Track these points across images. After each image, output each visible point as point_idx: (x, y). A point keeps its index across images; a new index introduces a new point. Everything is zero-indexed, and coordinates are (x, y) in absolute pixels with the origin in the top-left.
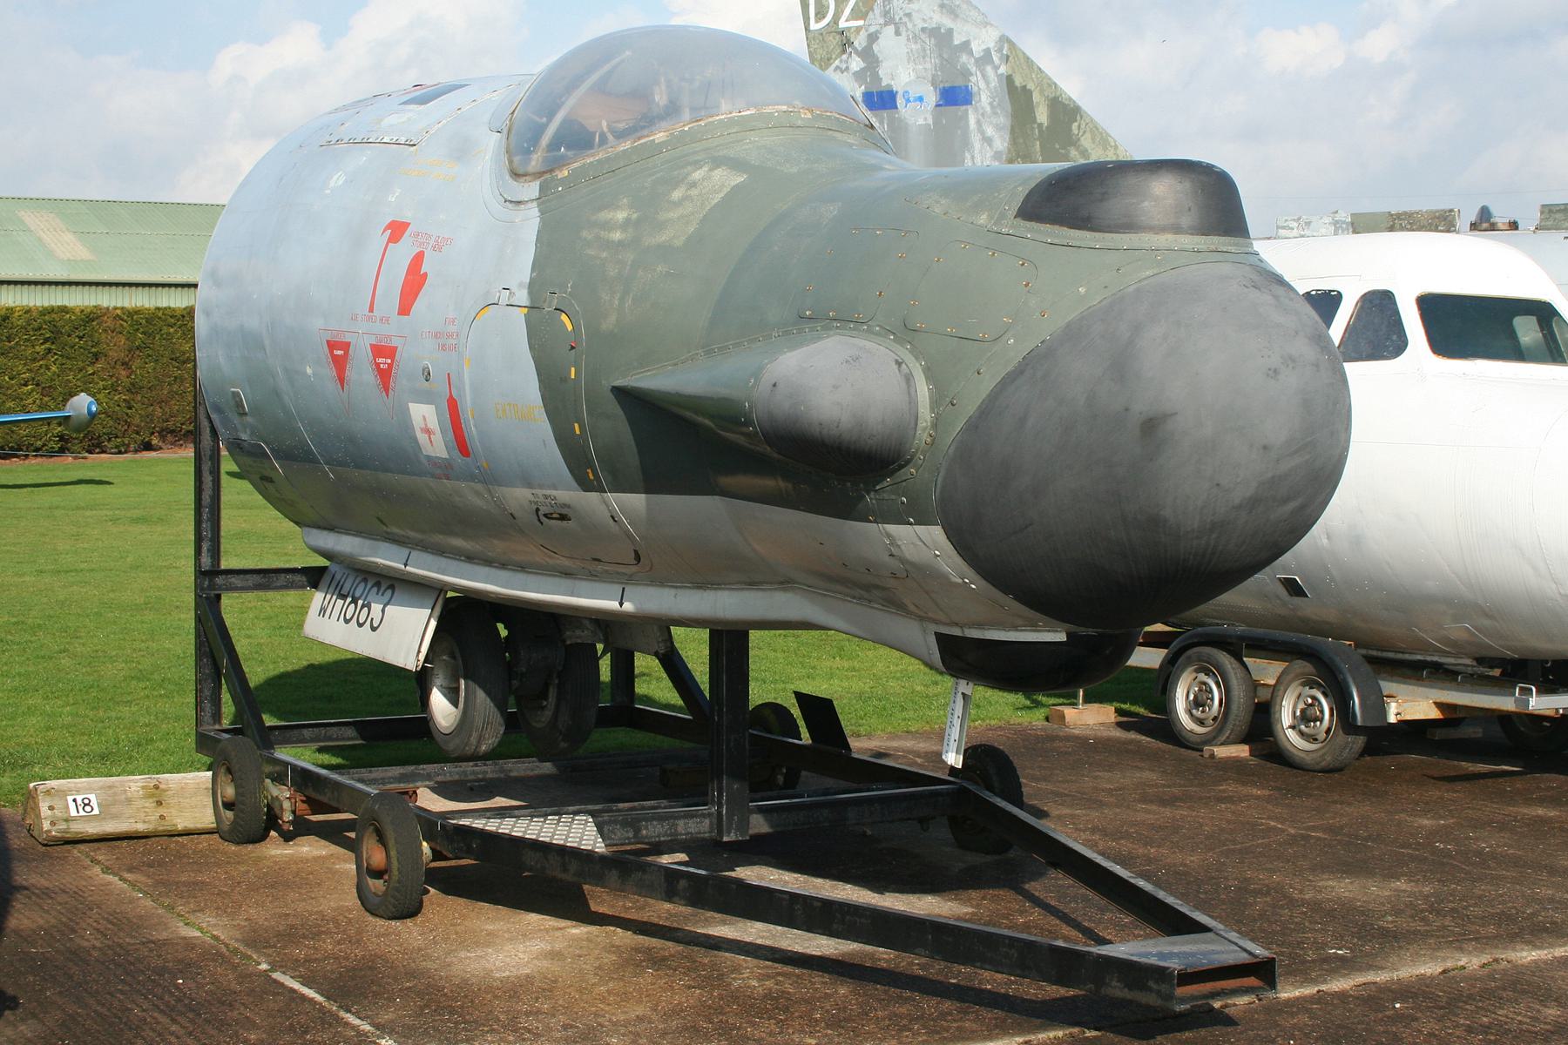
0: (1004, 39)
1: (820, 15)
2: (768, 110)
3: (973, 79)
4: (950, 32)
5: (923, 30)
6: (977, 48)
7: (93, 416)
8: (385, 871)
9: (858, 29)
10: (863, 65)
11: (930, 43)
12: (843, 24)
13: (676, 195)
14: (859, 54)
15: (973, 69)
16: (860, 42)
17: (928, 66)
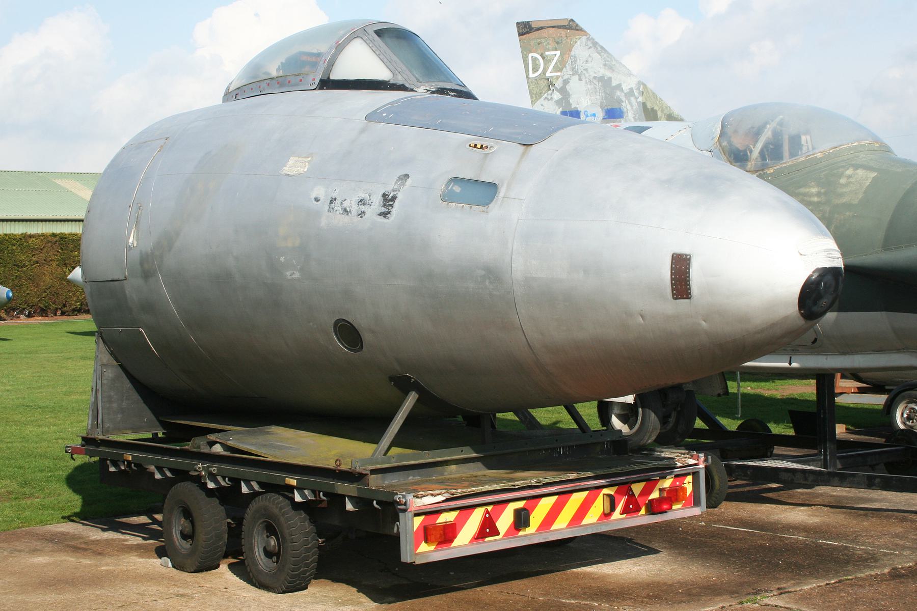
0: (640, 83)
1: (535, 69)
2: (863, 143)
3: (624, 104)
4: (610, 78)
5: (595, 78)
6: (625, 88)
7: (9, 298)
8: (275, 554)
9: (557, 77)
10: (560, 96)
11: (599, 85)
12: (548, 74)
13: (843, 181)
14: (558, 91)
15: (624, 99)
16: (558, 84)
17: (598, 97)
